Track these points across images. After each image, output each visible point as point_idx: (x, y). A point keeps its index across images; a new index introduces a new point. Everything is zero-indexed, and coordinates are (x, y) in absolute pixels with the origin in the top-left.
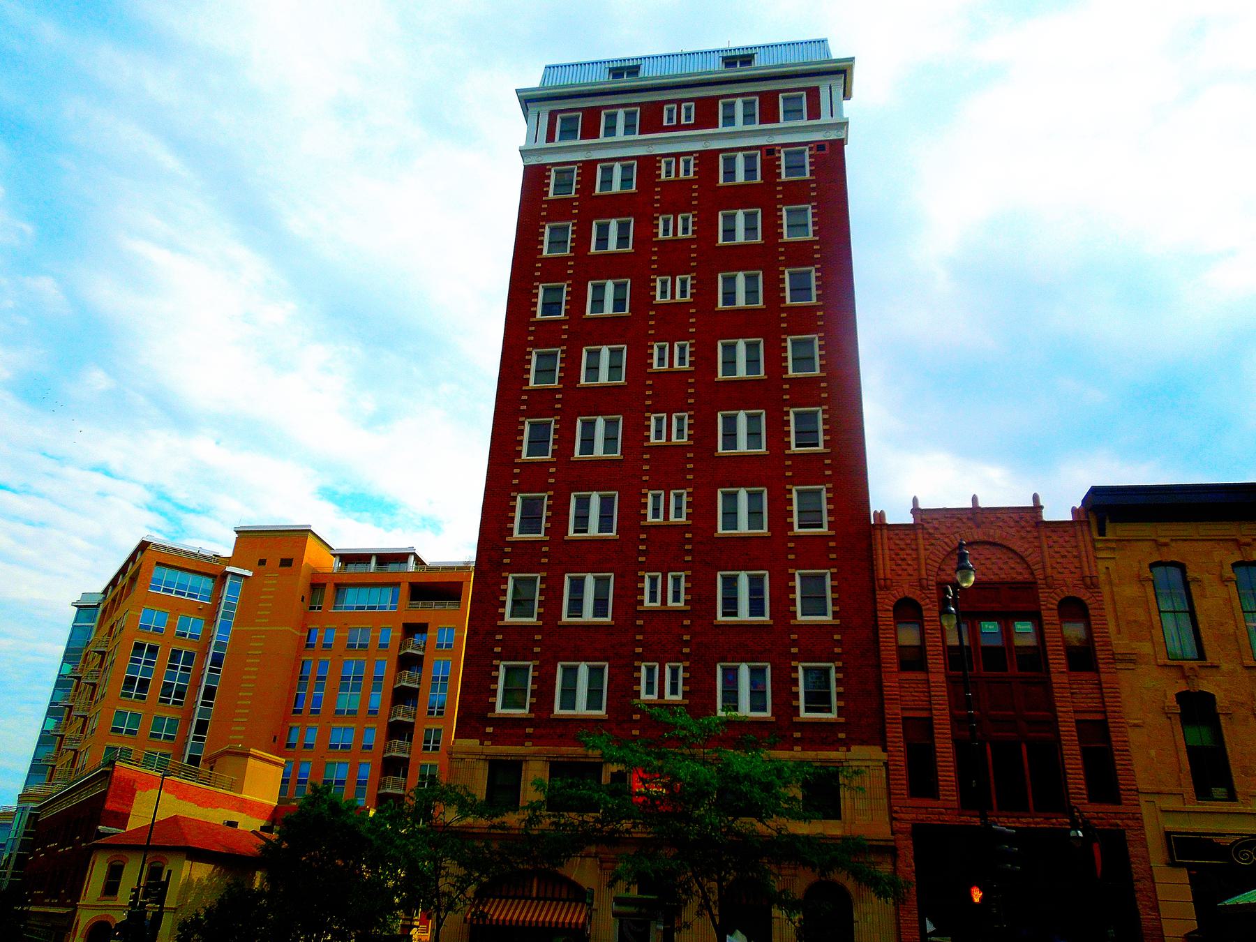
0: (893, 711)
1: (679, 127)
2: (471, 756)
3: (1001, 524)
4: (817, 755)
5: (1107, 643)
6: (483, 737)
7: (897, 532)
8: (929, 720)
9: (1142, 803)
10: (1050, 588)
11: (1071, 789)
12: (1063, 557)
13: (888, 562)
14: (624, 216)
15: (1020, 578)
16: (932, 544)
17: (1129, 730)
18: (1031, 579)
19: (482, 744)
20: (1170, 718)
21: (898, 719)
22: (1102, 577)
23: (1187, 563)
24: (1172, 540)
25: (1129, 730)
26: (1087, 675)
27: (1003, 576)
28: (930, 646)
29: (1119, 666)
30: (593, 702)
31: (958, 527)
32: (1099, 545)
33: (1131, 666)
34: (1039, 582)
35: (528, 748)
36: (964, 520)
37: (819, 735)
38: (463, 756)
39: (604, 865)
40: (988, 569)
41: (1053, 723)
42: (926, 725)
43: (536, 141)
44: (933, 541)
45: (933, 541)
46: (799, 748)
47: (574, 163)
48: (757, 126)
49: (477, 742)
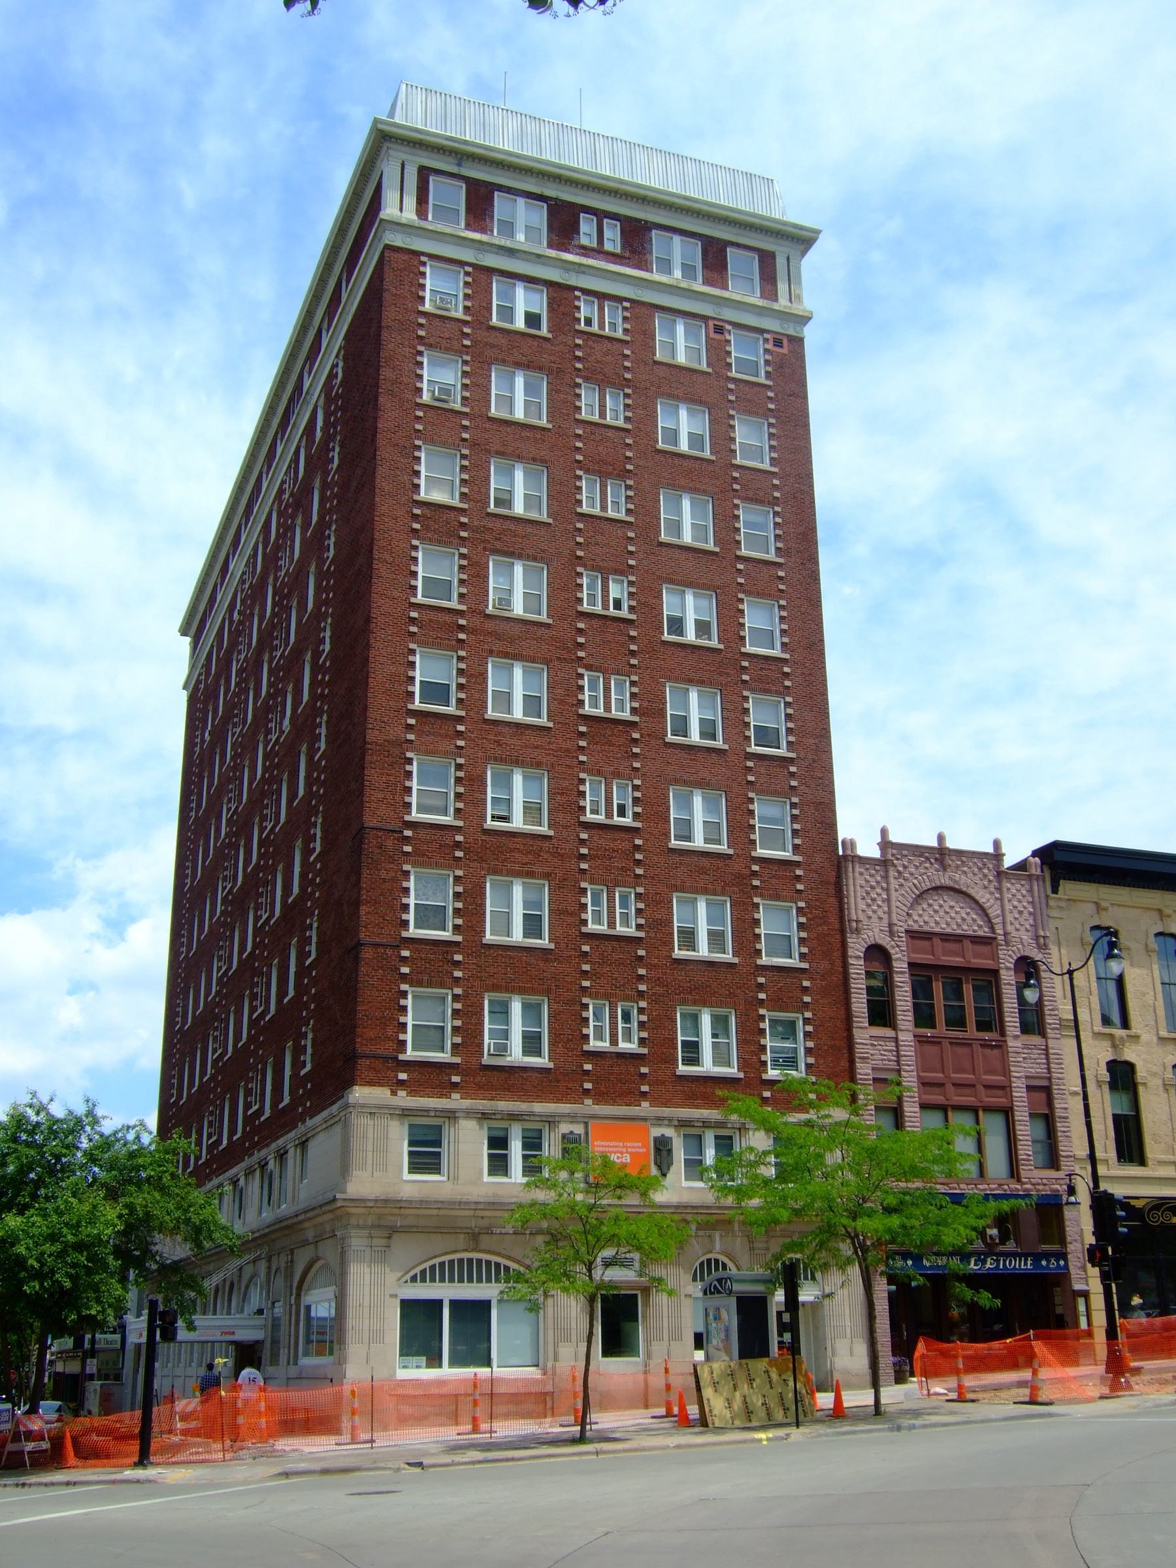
12: (1021, 913)
15: (980, 933)
19: (394, 1093)
24: (1112, 904)
26: (1036, 1040)
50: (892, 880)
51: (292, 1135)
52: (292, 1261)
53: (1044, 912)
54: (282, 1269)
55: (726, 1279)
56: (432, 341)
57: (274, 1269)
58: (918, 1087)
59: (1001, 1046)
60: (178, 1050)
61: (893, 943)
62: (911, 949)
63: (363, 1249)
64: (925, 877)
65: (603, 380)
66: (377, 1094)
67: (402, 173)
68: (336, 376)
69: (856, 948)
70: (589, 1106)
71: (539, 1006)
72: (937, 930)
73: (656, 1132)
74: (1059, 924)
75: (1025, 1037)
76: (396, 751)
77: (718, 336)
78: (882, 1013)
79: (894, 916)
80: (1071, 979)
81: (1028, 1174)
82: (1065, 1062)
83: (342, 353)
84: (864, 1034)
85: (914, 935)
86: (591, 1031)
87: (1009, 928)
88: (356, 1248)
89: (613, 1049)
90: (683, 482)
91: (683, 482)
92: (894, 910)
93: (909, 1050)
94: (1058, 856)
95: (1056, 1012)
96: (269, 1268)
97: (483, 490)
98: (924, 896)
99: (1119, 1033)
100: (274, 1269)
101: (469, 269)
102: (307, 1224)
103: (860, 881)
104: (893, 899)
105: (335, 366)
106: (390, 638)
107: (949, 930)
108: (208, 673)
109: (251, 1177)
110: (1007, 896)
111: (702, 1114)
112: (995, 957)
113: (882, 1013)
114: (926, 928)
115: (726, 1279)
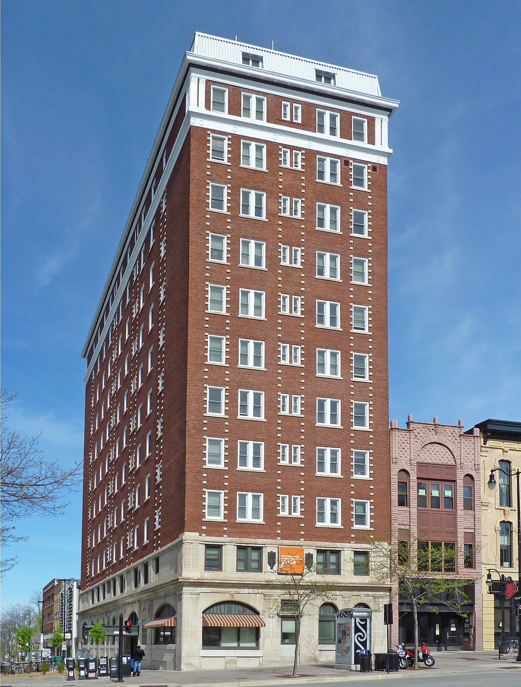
0: (395, 526)
1: (291, 124)
2: (196, 542)
3: (445, 434)
4: (362, 546)
5: (480, 498)
6: (201, 532)
7: (401, 433)
8: (409, 531)
9: (483, 568)
10: (462, 469)
11: (216, 554)
12: (469, 454)
13: (397, 449)
14: (260, 191)
15: (449, 463)
16: (416, 442)
17: (482, 537)
18: (454, 463)
19: (200, 535)
20: (496, 532)
21: (397, 529)
22: (482, 466)
23: (512, 461)
24: (510, 450)
25: (482, 537)
26: (470, 512)
27: (443, 461)
28: (412, 494)
29: (483, 508)
30: (255, 515)
31: (428, 434)
32: (483, 449)
33: (486, 508)
34: (458, 465)
35: (225, 539)
36: (431, 430)
37: (362, 536)
38: (192, 542)
39: (266, 597)
40: (437, 457)
41: (455, 533)
42: (408, 532)
43: (198, 105)
44: (417, 440)
45: (417, 440)
46: (303, 539)
47: (366, 162)
48: (264, 123)
49: (198, 534)
50: (412, 439)
51: (150, 555)
52: (152, 605)
53: (479, 453)
54: (147, 608)
55: (350, 611)
56: (213, 177)
57: (142, 608)
58: (417, 533)
59: (455, 515)
60: (90, 528)
61: (411, 468)
62: (418, 471)
63: (188, 599)
64: (427, 438)
65: (294, 193)
66: (195, 535)
67: (198, 85)
68: (162, 208)
69: (395, 470)
70: (279, 541)
71: (258, 497)
72: (431, 462)
73: (306, 552)
74: (484, 458)
75: (465, 511)
76: (199, 384)
77: (346, 167)
78: (403, 501)
79: (412, 456)
80: (518, 477)
81: (462, 570)
82: (482, 522)
83: (166, 194)
84: (396, 508)
85: (420, 465)
86: (280, 508)
87: (463, 461)
88: (186, 599)
89: (290, 516)
90: (327, 247)
91: (327, 247)
92: (412, 453)
93: (414, 516)
94: (490, 427)
95: (480, 500)
96: (140, 608)
97: (237, 256)
98: (426, 447)
99: (507, 509)
100: (142, 608)
101: (230, 137)
102: (161, 590)
103: (398, 440)
104: (412, 448)
105: (161, 203)
106: (196, 330)
107: (435, 462)
108: (96, 371)
109: (129, 574)
110: (463, 445)
111: (326, 544)
112: (455, 474)
113: (403, 501)
114: (426, 461)
115: (350, 611)
